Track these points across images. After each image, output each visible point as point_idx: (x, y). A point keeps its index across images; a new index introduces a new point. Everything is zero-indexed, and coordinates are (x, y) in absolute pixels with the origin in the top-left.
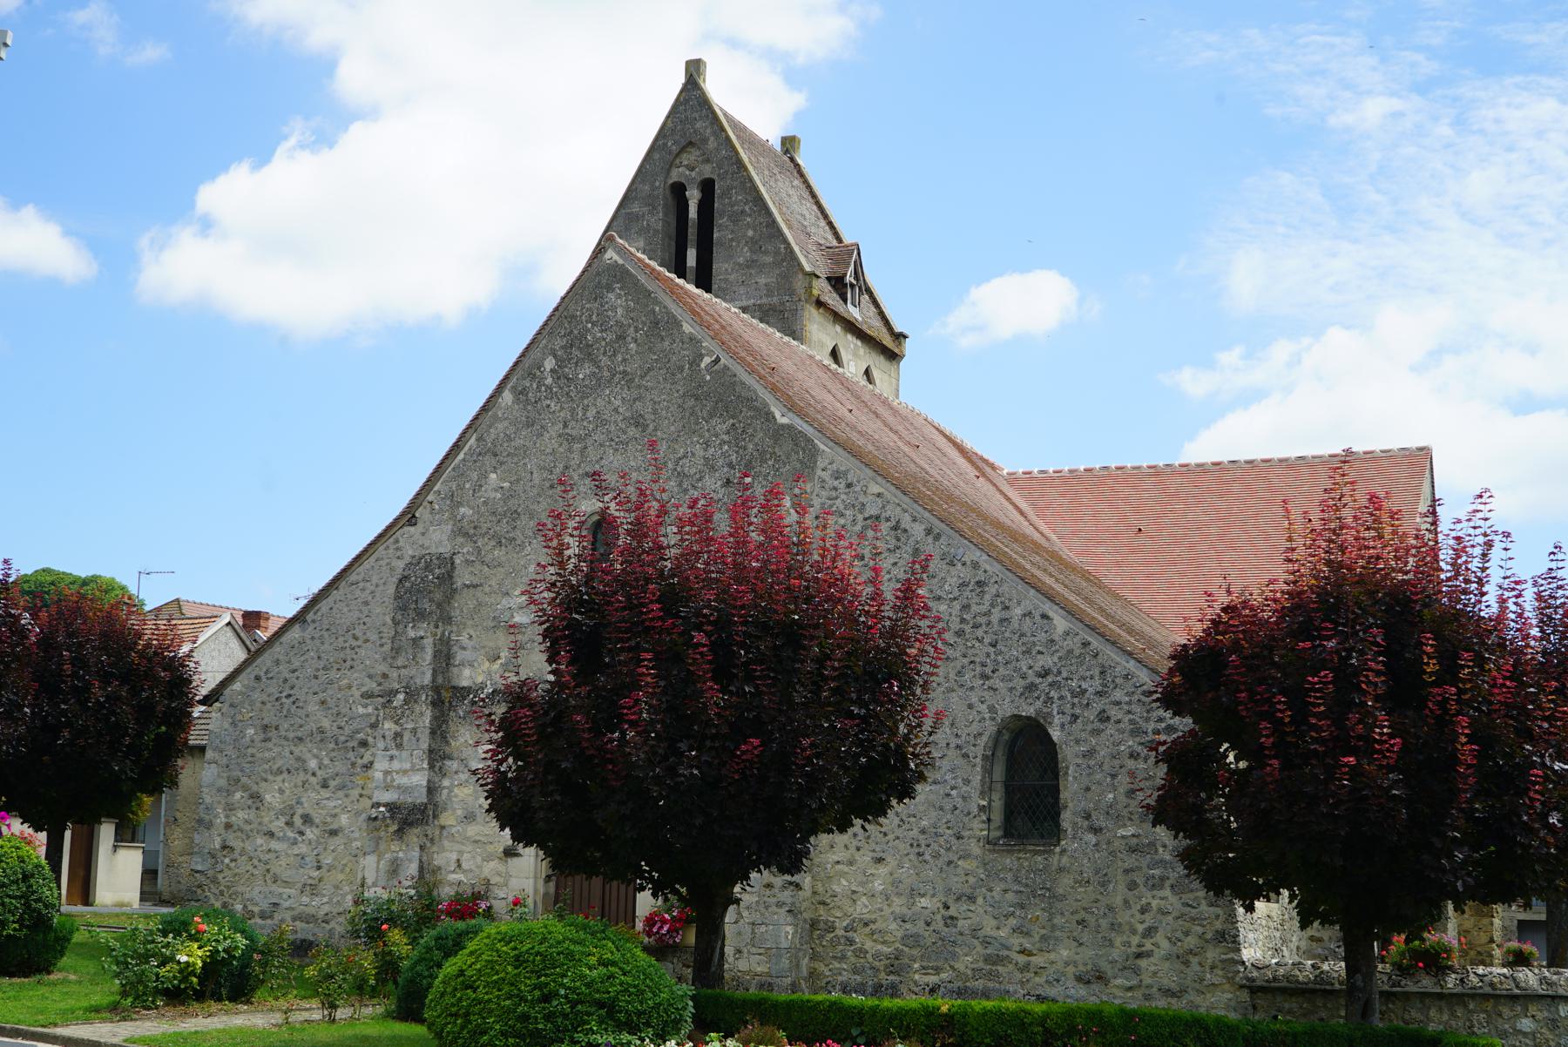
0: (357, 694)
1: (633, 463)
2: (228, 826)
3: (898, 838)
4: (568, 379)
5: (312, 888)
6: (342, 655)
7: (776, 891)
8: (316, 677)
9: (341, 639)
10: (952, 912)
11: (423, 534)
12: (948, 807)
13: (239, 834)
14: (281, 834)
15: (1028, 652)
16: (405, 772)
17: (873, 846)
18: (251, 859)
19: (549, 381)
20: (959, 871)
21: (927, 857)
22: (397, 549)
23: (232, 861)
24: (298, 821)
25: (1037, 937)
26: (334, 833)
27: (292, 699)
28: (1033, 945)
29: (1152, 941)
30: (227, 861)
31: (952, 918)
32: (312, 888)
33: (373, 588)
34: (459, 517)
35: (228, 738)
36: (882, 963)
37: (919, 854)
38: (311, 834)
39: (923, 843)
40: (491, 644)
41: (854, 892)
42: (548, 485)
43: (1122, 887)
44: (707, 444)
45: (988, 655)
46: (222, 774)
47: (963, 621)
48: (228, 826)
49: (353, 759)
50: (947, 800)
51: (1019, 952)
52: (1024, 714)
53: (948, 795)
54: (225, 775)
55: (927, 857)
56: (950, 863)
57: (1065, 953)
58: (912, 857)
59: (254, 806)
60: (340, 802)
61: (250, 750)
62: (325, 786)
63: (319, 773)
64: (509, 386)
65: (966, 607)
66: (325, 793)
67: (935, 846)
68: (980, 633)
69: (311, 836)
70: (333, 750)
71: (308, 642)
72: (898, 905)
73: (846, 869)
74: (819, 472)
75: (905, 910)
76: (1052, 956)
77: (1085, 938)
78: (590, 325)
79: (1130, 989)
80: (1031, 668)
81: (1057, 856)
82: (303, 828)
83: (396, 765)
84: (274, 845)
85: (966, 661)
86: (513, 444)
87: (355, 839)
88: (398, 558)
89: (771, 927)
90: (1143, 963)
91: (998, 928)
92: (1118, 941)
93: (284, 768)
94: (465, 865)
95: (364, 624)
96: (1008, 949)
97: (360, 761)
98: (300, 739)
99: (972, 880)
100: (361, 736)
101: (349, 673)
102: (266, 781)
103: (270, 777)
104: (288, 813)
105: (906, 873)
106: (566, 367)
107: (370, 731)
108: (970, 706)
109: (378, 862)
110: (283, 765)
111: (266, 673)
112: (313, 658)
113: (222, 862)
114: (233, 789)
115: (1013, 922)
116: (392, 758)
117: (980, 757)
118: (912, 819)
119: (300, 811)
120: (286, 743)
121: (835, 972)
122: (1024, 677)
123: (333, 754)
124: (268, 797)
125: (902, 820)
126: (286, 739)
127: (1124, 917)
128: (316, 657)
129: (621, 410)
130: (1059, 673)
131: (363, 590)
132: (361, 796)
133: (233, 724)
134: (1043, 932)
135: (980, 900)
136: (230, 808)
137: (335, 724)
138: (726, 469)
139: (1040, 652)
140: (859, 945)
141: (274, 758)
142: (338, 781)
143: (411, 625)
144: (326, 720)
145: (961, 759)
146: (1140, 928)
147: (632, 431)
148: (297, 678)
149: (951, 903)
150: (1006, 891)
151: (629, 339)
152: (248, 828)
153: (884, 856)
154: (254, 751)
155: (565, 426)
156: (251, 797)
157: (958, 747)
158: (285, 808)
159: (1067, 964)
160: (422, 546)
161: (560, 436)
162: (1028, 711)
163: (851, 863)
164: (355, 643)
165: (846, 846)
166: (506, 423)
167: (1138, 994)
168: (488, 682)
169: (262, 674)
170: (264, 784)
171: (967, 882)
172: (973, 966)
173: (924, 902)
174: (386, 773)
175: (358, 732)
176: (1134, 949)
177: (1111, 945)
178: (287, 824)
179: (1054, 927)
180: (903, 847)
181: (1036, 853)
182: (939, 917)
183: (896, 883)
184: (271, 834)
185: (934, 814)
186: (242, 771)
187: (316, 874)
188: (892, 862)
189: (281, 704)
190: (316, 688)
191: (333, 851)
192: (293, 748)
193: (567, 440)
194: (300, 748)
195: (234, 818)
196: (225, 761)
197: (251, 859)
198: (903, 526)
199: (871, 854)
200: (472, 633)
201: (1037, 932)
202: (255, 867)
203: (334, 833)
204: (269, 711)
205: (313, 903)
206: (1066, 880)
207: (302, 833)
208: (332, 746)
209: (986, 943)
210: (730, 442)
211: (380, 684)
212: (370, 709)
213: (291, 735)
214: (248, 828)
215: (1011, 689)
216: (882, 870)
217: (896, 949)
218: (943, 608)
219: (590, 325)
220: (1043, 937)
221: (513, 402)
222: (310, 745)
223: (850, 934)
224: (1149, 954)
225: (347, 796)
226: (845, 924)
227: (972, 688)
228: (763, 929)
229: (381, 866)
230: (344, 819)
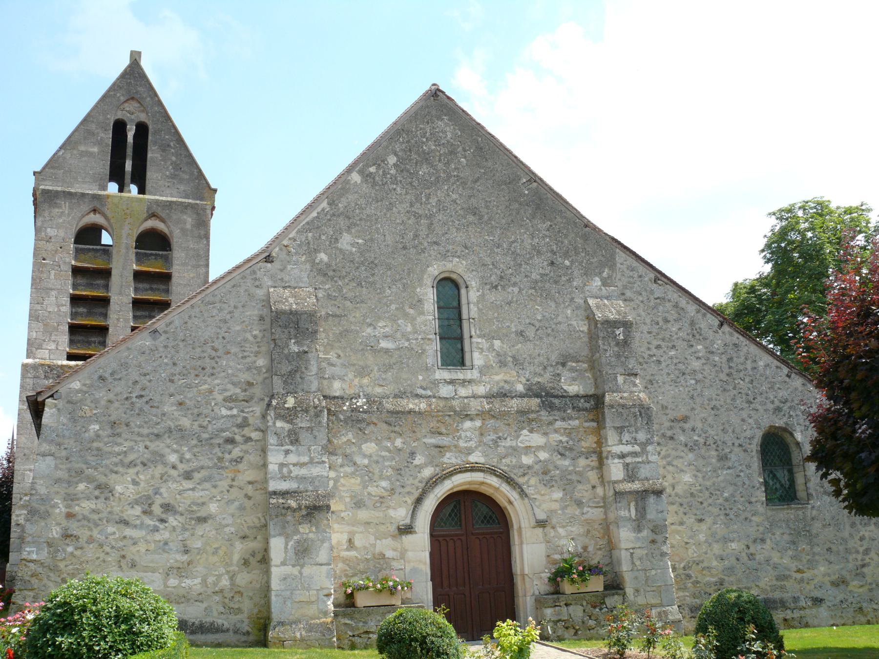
0: (220, 398)
1: (473, 240)
2: (70, 516)
3: (711, 505)
4: (410, 173)
5: (180, 571)
6: (199, 363)
7: (659, 545)
8: (172, 381)
9: (198, 350)
10: (752, 550)
11: (281, 270)
12: (740, 484)
13: (85, 523)
14: (138, 522)
15: (772, 388)
16: (302, 465)
17: (695, 511)
18: (101, 546)
19: (393, 171)
20: (754, 524)
21: (732, 516)
22: (256, 279)
23: (76, 549)
24: (157, 509)
25: (805, 561)
26: (203, 520)
27: (144, 400)
28: (803, 566)
29: (869, 556)
30: (70, 549)
31: (752, 554)
32: (180, 571)
33: (231, 309)
34: (317, 261)
35: (67, 433)
36: (712, 589)
37: (727, 515)
38: (172, 521)
39: (727, 507)
40: (361, 363)
41: (687, 543)
42: (400, 246)
43: (848, 527)
44: (533, 237)
45: (749, 389)
46: (61, 466)
47: (730, 367)
48: (70, 516)
49: (220, 454)
50: (738, 479)
51: (795, 572)
52: (777, 425)
53: (738, 476)
54: (64, 467)
55: (732, 516)
56: (746, 519)
57: (822, 569)
58: (722, 517)
59: (103, 496)
60: (207, 492)
61: (95, 445)
62: (188, 476)
63: (181, 467)
64: (357, 169)
65: (730, 360)
66: (187, 484)
67: (735, 509)
68: (741, 375)
69: (175, 523)
70: (196, 446)
71: (161, 349)
72: (717, 548)
73: (679, 528)
74: (618, 265)
75: (721, 552)
76: (816, 571)
77: (832, 558)
78: (424, 140)
79: (862, 586)
80: (776, 397)
81: (809, 510)
82: (164, 516)
83: (292, 458)
84: (128, 532)
85: (735, 392)
86: (365, 212)
87: (227, 525)
88: (257, 287)
89: (659, 571)
90: (865, 570)
91: (782, 558)
92: (851, 558)
93: (138, 461)
94: (358, 543)
95: (223, 338)
96: (789, 570)
97: (227, 456)
98: (158, 436)
99: (761, 529)
100: (227, 434)
101: (209, 380)
102: (116, 473)
103: (121, 469)
104: (146, 504)
105: (720, 529)
106: (407, 164)
107: (236, 430)
108: (743, 420)
109: (287, 544)
110: (138, 458)
111: (112, 374)
112: (166, 364)
113: (64, 551)
114: (75, 480)
115: (790, 553)
116: (287, 452)
117: (755, 451)
118: (718, 492)
119: (158, 501)
120: (139, 439)
121: (682, 599)
122: (773, 402)
123: (195, 450)
124: (119, 489)
125: (711, 493)
126: (139, 434)
127: (851, 544)
128: (170, 363)
129: (458, 201)
130: (793, 401)
131: (220, 310)
132: (231, 486)
133: (74, 420)
134: (808, 557)
135: (768, 541)
136: (71, 498)
137: (196, 423)
138: (549, 255)
139: (779, 389)
140: (695, 579)
141: (125, 452)
142: (204, 473)
143: (293, 341)
144: (185, 419)
145: (742, 453)
146: (861, 550)
147: (471, 218)
148: (150, 381)
149: (751, 545)
150: (783, 534)
151: (459, 155)
152: (95, 517)
153: (703, 517)
154: (101, 445)
155: (412, 205)
156: (98, 487)
157: (740, 445)
158: (140, 498)
159: (824, 576)
160: (282, 279)
161: (408, 212)
162: (779, 423)
163: (681, 523)
164: (213, 354)
165: (676, 512)
166: (356, 196)
167: (866, 588)
168: (361, 394)
169: (107, 375)
170: (114, 476)
171: (758, 530)
172: (770, 584)
173: (734, 545)
174: (282, 465)
175: (223, 430)
176: (860, 563)
177: (848, 562)
178: (145, 512)
179: (814, 554)
180: (716, 511)
181: (798, 509)
182: (744, 554)
183: (713, 535)
184: (126, 523)
185: (731, 489)
186: (87, 463)
187: (185, 558)
188: (709, 520)
189: (132, 403)
190: (172, 390)
191: (202, 536)
192: (148, 443)
193: (415, 216)
194: (157, 443)
195: (77, 508)
196: (64, 453)
197: (101, 546)
198: (681, 306)
199: (694, 517)
200: (340, 352)
201: (805, 558)
202: (107, 553)
203: (203, 520)
204: (117, 409)
205: (183, 585)
206: (816, 525)
207: (163, 521)
208: (194, 442)
209: (775, 567)
210: (550, 237)
211: (245, 390)
212: (235, 411)
213: (145, 431)
214: (95, 517)
215: (766, 410)
216: (704, 527)
217: (720, 579)
218: (717, 359)
219: (424, 140)
220: (808, 560)
221: (362, 182)
222: (168, 441)
223: (686, 572)
224: (867, 565)
225: (215, 487)
226: (682, 565)
227: (742, 409)
228: (653, 572)
229: (289, 547)
230: (213, 508)
